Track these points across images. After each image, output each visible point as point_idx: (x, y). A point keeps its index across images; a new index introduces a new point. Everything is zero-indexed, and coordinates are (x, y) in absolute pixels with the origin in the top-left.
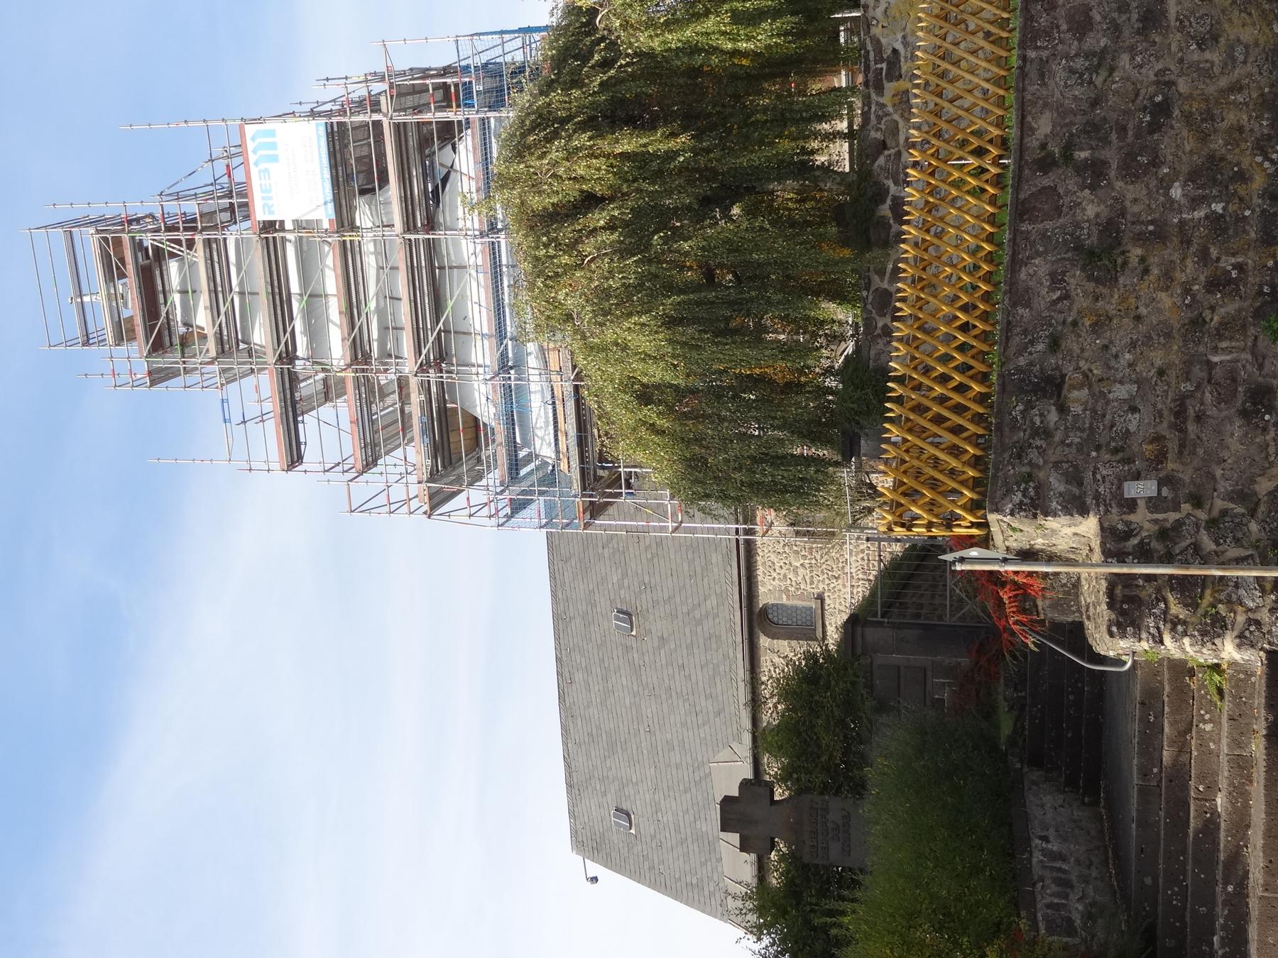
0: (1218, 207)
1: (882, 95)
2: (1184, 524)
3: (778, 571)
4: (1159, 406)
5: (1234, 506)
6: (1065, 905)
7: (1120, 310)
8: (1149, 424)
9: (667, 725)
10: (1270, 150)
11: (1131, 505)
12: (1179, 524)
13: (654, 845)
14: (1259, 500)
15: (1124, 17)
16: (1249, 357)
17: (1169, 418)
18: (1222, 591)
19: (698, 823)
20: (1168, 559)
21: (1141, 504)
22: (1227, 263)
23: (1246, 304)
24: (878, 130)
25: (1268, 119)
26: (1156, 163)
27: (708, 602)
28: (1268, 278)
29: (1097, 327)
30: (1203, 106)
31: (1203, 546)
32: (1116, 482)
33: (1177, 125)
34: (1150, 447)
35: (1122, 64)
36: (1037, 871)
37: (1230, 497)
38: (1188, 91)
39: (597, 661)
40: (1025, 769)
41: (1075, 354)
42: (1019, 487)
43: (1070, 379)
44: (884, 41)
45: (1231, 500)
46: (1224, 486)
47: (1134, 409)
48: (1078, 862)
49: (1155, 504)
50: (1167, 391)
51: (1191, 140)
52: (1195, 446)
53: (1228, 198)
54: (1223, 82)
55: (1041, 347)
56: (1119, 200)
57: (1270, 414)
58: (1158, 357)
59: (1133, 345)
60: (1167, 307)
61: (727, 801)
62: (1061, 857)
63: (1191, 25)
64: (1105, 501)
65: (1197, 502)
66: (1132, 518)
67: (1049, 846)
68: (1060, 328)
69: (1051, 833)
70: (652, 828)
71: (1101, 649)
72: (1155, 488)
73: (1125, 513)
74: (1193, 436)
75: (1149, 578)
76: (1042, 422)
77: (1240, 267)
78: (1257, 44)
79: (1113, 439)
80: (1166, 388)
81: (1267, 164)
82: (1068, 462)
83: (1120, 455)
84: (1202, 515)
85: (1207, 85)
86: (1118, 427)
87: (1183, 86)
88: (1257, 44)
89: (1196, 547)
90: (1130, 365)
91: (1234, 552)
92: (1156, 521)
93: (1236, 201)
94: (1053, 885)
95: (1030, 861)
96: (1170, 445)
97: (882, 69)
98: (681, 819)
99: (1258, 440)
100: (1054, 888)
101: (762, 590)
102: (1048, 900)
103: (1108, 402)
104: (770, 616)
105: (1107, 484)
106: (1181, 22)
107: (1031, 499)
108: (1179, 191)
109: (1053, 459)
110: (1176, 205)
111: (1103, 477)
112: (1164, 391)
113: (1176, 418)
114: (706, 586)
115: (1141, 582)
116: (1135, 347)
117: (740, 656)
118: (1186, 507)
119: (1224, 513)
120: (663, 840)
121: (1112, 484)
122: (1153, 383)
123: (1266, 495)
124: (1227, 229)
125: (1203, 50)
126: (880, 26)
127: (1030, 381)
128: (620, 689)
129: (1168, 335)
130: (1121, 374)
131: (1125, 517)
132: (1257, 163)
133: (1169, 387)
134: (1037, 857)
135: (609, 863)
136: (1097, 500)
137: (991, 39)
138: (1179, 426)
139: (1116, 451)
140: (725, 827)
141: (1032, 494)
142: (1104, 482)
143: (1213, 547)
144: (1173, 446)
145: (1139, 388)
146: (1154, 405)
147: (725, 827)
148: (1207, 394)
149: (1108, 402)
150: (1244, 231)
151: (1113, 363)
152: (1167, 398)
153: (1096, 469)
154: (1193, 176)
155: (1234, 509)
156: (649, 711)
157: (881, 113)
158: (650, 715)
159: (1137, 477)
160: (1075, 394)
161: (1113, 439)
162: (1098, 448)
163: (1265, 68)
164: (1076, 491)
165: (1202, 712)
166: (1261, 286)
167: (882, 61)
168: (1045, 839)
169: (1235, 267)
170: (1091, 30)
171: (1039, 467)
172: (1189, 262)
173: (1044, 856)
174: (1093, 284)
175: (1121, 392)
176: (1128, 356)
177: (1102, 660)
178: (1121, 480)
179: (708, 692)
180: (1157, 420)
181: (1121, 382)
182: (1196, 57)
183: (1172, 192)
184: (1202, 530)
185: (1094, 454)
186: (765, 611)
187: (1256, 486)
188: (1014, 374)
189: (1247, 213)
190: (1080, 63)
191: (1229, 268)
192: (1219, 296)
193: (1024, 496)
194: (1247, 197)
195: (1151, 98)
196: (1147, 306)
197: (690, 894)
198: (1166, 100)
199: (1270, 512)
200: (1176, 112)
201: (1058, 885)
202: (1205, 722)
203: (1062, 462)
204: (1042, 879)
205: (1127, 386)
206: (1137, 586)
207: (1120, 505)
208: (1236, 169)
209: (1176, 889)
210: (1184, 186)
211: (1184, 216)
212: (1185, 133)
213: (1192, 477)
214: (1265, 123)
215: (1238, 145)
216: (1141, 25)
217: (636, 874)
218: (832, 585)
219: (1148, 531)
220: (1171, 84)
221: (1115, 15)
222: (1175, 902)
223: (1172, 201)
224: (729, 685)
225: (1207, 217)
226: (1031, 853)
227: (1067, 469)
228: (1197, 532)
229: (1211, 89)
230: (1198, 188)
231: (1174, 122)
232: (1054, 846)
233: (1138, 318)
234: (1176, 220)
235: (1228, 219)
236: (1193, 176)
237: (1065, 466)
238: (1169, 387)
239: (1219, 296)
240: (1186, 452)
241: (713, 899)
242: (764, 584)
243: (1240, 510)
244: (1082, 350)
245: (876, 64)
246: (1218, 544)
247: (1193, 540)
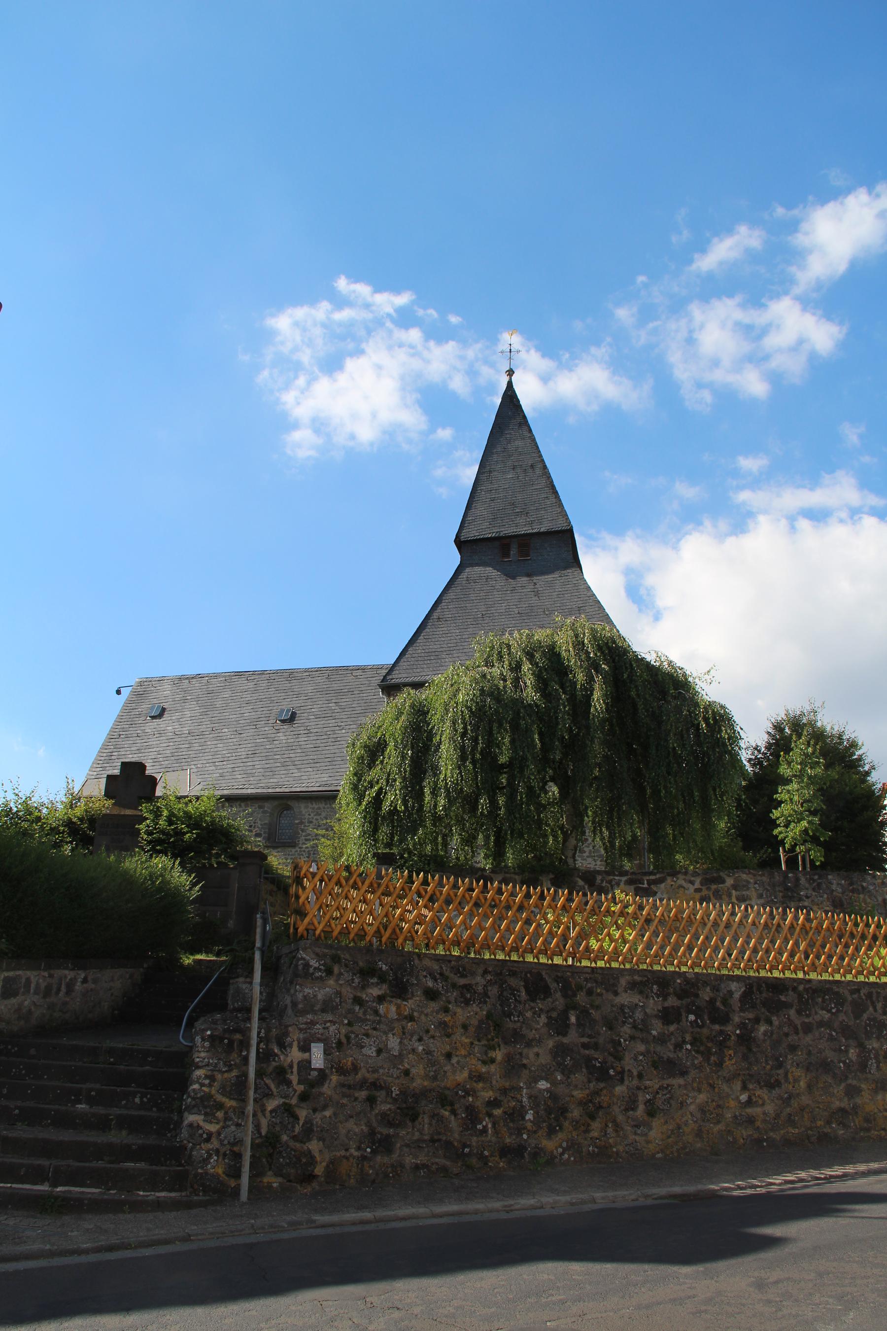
0: (529, 1116)
1: (625, 884)
2: (288, 1087)
3: (315, 817)
4: (381, 1071)
5: (301, 1124)
6: (29, 991)
7: (456, 1043)
8: (367, 1063)
9: (216, 742)
10: (570, 1152)
11: (305, 1048)
12: (289, 1083)
13: (139, 732)
14: (305, 1144)
15: (671, 1047)
16: (415, 1138)
17: (371, 1077)
18: (235, 1114)
19: (151, 761)
20: (260, 1074)
21: (306, 1055)
22: (487, 1122)
23: (456, 1136)
24: (602, 881)
25: (593, 1151)
26: (567, 1072)
27: (296, 771)
28: (475, 1151)
29: (443, 1025)
30: (605, 1105)
31: (270, 1101)
32: (324, 1037)
33: (591, 1085)
34: (349, 1063)
35: (638, 1046)
36: (58, 973)
37: (308, 1122)
38: (616, 1094)
39: (260, 697)
40: (141, 970)
41: (423, 1009)
42: (322, 965)
43: (405, 1005)
44: (663, 885)
45: (306, 1122)
46: (317, 1118)
47: (379, 1051)
48: (65, 1004)
49: (305, 1065)
50: (392, 1076)
51: (581, 1096)
52: (348, 1096)
53: (536, 1122)
54: (620, 1118)
55: (430, 984)
56: (540, 1041)
57: (371, 1153)
58: (418, 1070)
59: (428, 1052)
60: (457, 1078)
61: (141, 767)
62: (70, 990)
63: (663, 1095)
64: (309, 1028)
65: (304, 1097)
66: (295, 1048)
67: (79, 984)
68: (444, 998)
69: (90, 985)
70: (150, 731)
71: (199, 1025)
72: (318, 1066)
73: (299, 1043)
74: (357, 1095)
75: (246, 1060)
76: (372, 983)
77: (484, 1131)
78: (648, 1142)
79: (357, 1036)
80: (395, 1076)
81: (560, 1150)
82: (341, 1002)
83: (344, 1040)
84: (294, 1101)
85: (620, 1107)
86: (366, 1040)
87: (619, 1089)
88: (648, 1142)
89: (269, 1095)
90: (413, 1050)
91: (264, 1122)
92: (291, 1066)
93: (534, 1129)
94: (45, 984)
95: (66, 968)
96: (350, 1078)
97: (643, 884)
98: (154, 750)
99: (351, 1143)
100: (43, 985)
101: (302, 805)
102: (34, 980)
103: (386, 1033)
104: (285, 812)
105: (321, 1031)
106: (666, 1088)
107: (313, 974)
108: (543, 1087)
109: (343, 990)
110: (533, 1085)
111: (327, 1028)
112: (392, 1074)
113: (371, 1083)
114: (306, 770)
115: (244, 1053)
116: (427, 1054)
117: (259, 791)
118: (301, 1088)
119: (297, 1118)
120: (141, 738)
121: (322, 1034)
122: (400, 1067)
123: (308, 1148)
124: (513, 1121)
125: (645, 1104)
126: (673, 883)
127: (405, 976)
128: (242, 712)
129: (435, 1078)
130: (407, 1043)
131: (295, 1044)
132: (561, 1143)
133: (396, 1078)
134: (70, 974)
135: (129, 702)
136: (310, 1023)
137: (673, 953)
138: (363, 1084)
139: (348, 1038)
140: (124, 764)
141: (317, 975)
142: (324, 1028)
143: (269, 1108)
144: (350, 1079)
145: (395, 1056)
146: (382, 1067)
147: (124, 764)
148: (388, 1106)
149: (386, 1033)
150: (511, 1134)
151: (415, 1037)
152: (387, 1076)
153: (333, 1023)
154: (554, 1097)
155: (298, 1124)
156: (226, 730)
157: (613, 883)
158: (223, 731)
159: (326, 1053)
160: (393, 1009)
161: (357, 1036)
162: (350, 1024)
163: (631, 1148)
164: (317, 1007)
165: (149, 1096)
166: (469, 1146)
167: (649, 883)
168: (85, 981)
169: (485, 1127)
170: (663, 1024)
171: (337, 981)
172: (491, 1093)
173: (71, 980)
174: (476, 1023)
175: (393, 1043)
176: (421, 1048)
177: (191, 1024)
178: (324, 1040)
179: (236, 769)
180: (370, 1069)
181: (400, 1043)
182: (640, 1098)
183: (544, 1082)
184: (284, 1100)
185: (346, 1022)
186: (288, 808)
187: (316, 1141)
188: (410, 964)
189: (525, 1136)
190: (639, 1015)
191: (484, 1123)
192: (463, 1115)
193: (315, 968)
194: (537, 1135)
195: (613, 1068)
196: (458, 1062)
197: (105, 755)
198: (611, 1077)
199: (295, 1151)
200: (602, 1085)
201: (46, 987)
202: (141, 1098)
203: (341, 997)
204: (51, 976)
205: (397, 1048)
206: (241, 1051)
207: (305, 1040)
208: (557, 1128)
209: (24, 1072)
210: (547, 1090)
211: (525, 1090)
212: (587, 1091)
213: (324, 1094)
214: (591, 1148)
215: (575, 1130)
216: (665, 1059)
217: (119, 720)
218: (304, 854)
219: (285, 1060)
220: (622, 1081)
221: (673, 1041)
222: (14, 1070)
223: (536, 1082)
224: (240, 783)
225: (522, 1107)
226: (73, 969)
227: (335, 1001)
228: (281, 1097)
229: (616, 1110)
230: (545, 1101)
231: (594, 1083)
232: (78, 986)
233: (449, 1056)
234: (522, 1085)
235: (521, 1122)
236: (554, 1097)
237: (338, 1000)
238: (396, 1078)
239: (463, 1115)
240: (344, 1090)
241: (101, 769)
242: (306, 807)
243: (297, 1129)
244: (427, 1015)
245: (647, 880)
246: (271, 1112)
247: (275, 1093)
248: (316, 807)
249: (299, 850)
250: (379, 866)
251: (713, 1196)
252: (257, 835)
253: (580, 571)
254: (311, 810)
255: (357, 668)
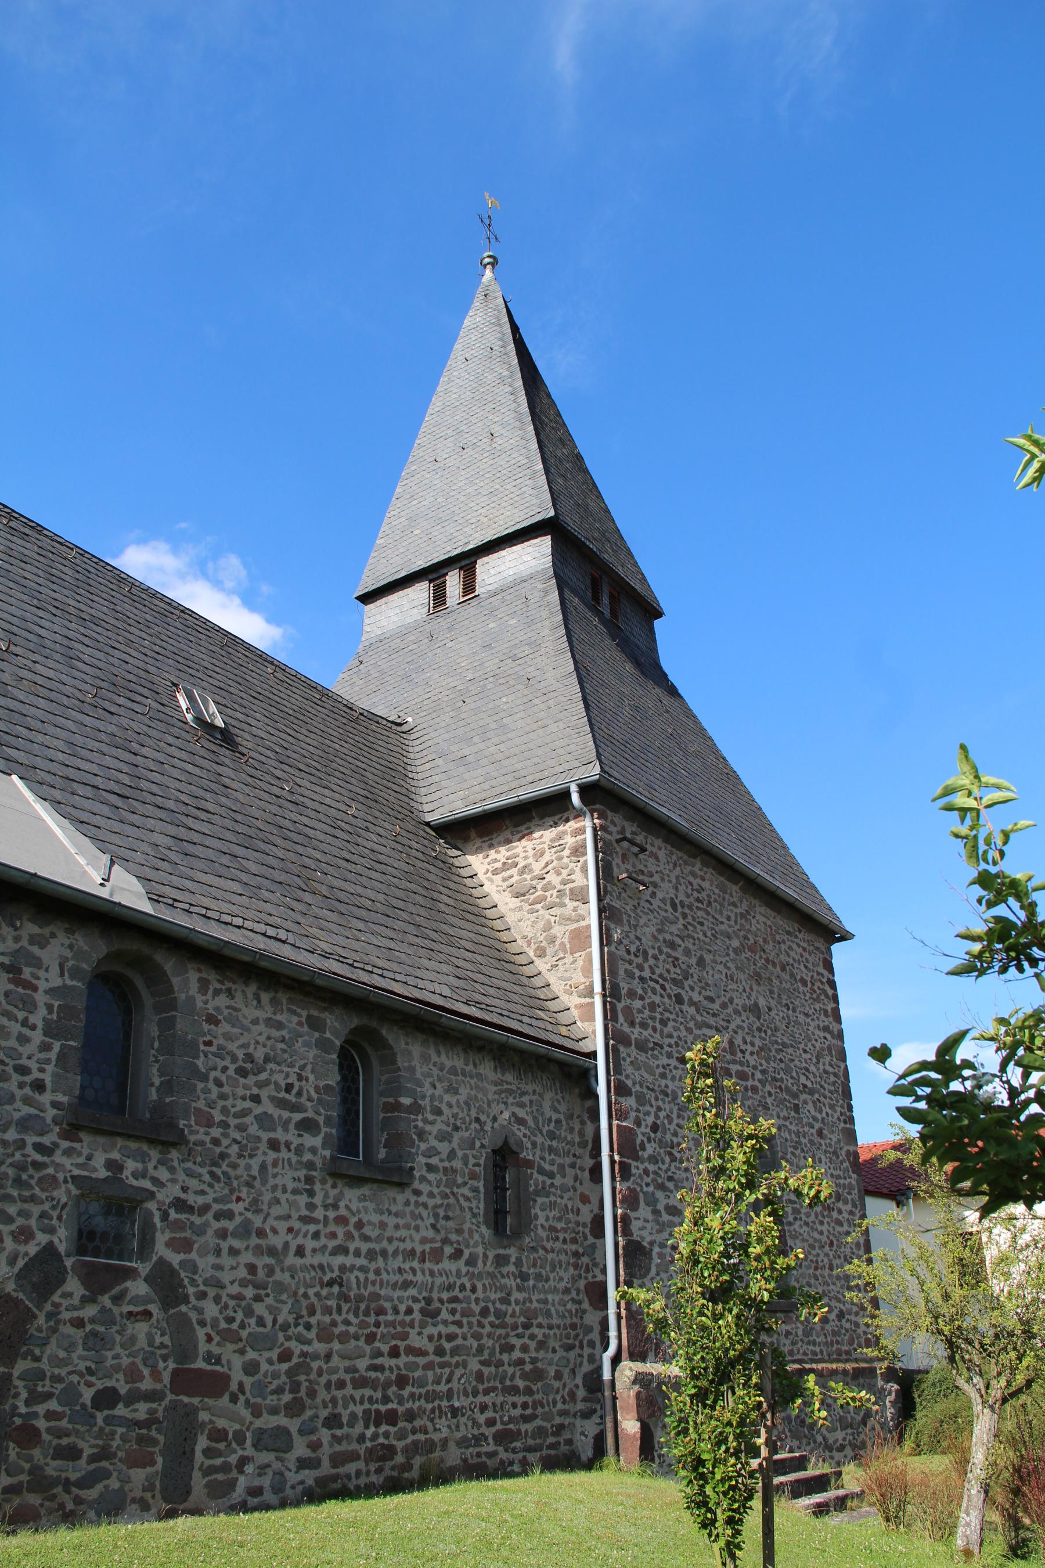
242: (426, 1059)
248: (448, 1063)
249: (413, 1199)
250: (327, 1177)
251: (188, 1369)
252: (307, 1126)
253: (667, 700)
254: (435, 1071)
255: (314, 685)
